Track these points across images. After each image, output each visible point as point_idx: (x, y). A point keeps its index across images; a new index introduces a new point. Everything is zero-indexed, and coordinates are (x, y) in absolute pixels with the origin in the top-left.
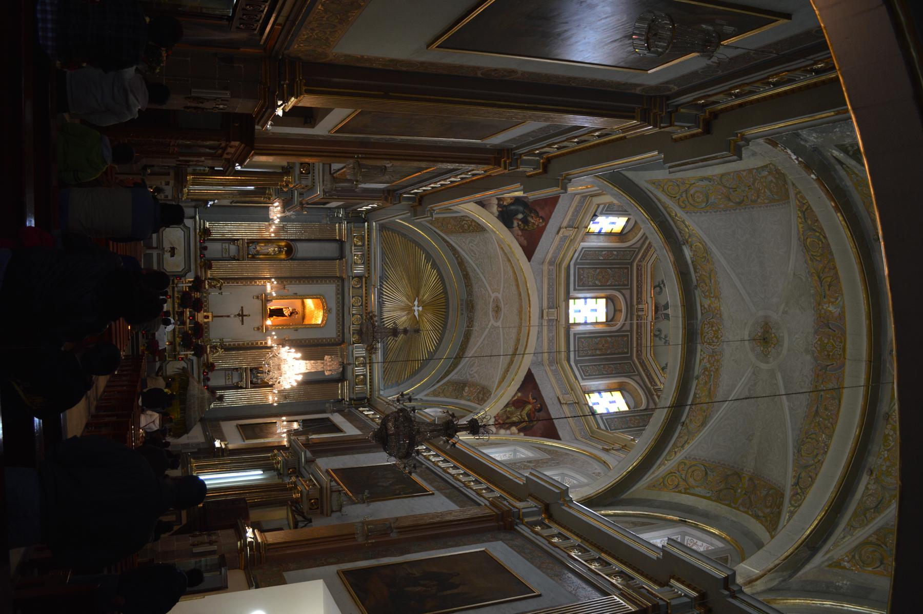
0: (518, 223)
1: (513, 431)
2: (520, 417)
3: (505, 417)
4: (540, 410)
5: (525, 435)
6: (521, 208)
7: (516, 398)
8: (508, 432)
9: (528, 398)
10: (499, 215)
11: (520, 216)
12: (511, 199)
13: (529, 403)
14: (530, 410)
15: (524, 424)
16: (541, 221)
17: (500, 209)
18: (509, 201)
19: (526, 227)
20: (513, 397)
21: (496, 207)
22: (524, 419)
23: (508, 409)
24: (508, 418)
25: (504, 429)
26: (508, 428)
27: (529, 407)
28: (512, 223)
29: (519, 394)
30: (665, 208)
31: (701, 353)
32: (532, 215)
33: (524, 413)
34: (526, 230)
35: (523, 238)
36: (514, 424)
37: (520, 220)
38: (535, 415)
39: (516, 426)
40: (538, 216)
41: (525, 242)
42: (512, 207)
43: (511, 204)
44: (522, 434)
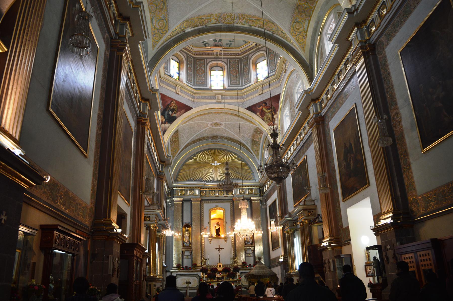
1: (276, 117)
3: (269, 121)
4: (266, 104)
6: (166, 112)
7: (260, 115)
8: (276, 119)
11: (170, 113)
13: (262, 109)
16: (173, 102)
17: (167, 123)
19: (176, 110)
20: (260, 117)
21: (166, 125)
23: (265, 119)
24: (269, 119)
26: (275, 119)
27: (264, 109)
28: (174, 117)
29: (258, 114)
32: (170, 107)
34: (177, 110)
36: (273, 116)
37: (172, 113)
40: (170, 104)
42: (166, 116)
44: (277, 112)
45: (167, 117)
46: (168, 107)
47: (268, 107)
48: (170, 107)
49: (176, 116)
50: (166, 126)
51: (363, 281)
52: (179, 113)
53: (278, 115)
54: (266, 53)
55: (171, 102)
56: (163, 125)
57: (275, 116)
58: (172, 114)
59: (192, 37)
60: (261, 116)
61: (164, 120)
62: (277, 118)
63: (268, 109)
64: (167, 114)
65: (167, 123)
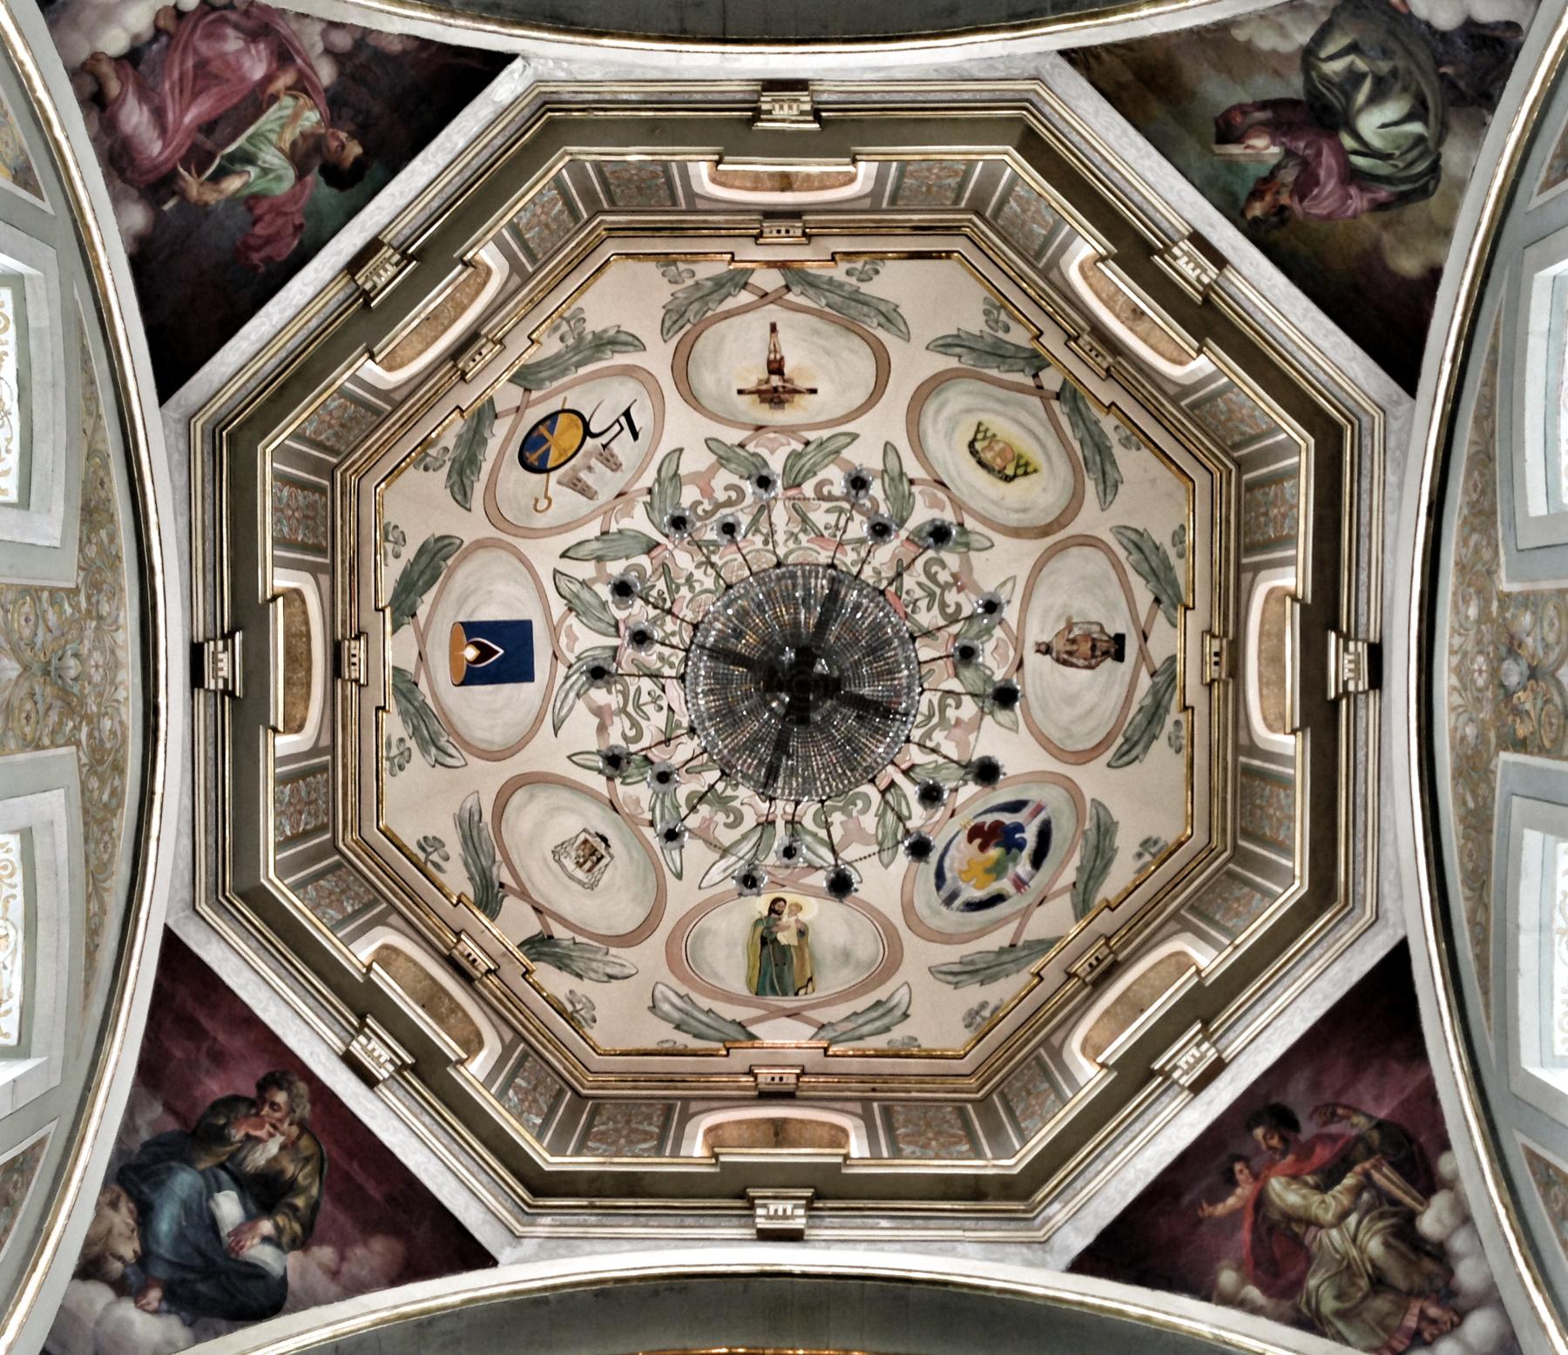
0: (266, 1240)
1: (1448, 1219)
2: (1352, 1220)
3: (1382, 1304)
4: (1284, 1120)
5: (1445, 1145)
6: (184, 1181)
7: (1253, 1293)
8: (1459, 1243)
9: (1235, 1214)
10: (190, 1324)
11: (229, 1207)
12: (114, 1205)
13: (1261, 1201)
14: (1295, 1177)
15: (1386, 1178)
16: (281, 1097)
17: (154, 1295)
18: (123, 1219)
19: (300, 1202)
20: (1255, 1310)
21: (128, 1310)
22: (1357, 1191)
23: (1328, 1305)
24: (1379, 1282)
25: (1450, 1273)
26: (1439, 1254)
27: (1286, 1194)
28: (256, 1272)
29: (1227, 1278)
30: (334, 1337)
31: (823, 1244)
32: (237, 1134)
33: (1326, 1205)
34: (315, 1207)
35: (359, 1251)
36: (1405, 1232)
37: (251, 1218)
38: (1320, 1138)
39: (1411, 1217)
40: (252, 1103)
41: (379, 1244)
42: (165, 1224)
43: (145, 1215)
44: (1445, 1165)
45: (180, 1237)
46: (220, 1137)
47: (1323, 1154)
48: (237, 1134)
49: (283, 1281)
50: (131, 1324)
51: (901, 968)
52: (325, 1253)
53: (1469, 1187)
54: (917, 562)
55: (266, 1085)
56: (99, 1296)
57: (1432, 1220)
58: (237, 1232)
59: (429, 597)
60: (1266, 1290)
61: (128, 1249)
62: (1466, 1219)
63: (1328, 1179)
64: (186, 1207)
65: (154, 1295)
